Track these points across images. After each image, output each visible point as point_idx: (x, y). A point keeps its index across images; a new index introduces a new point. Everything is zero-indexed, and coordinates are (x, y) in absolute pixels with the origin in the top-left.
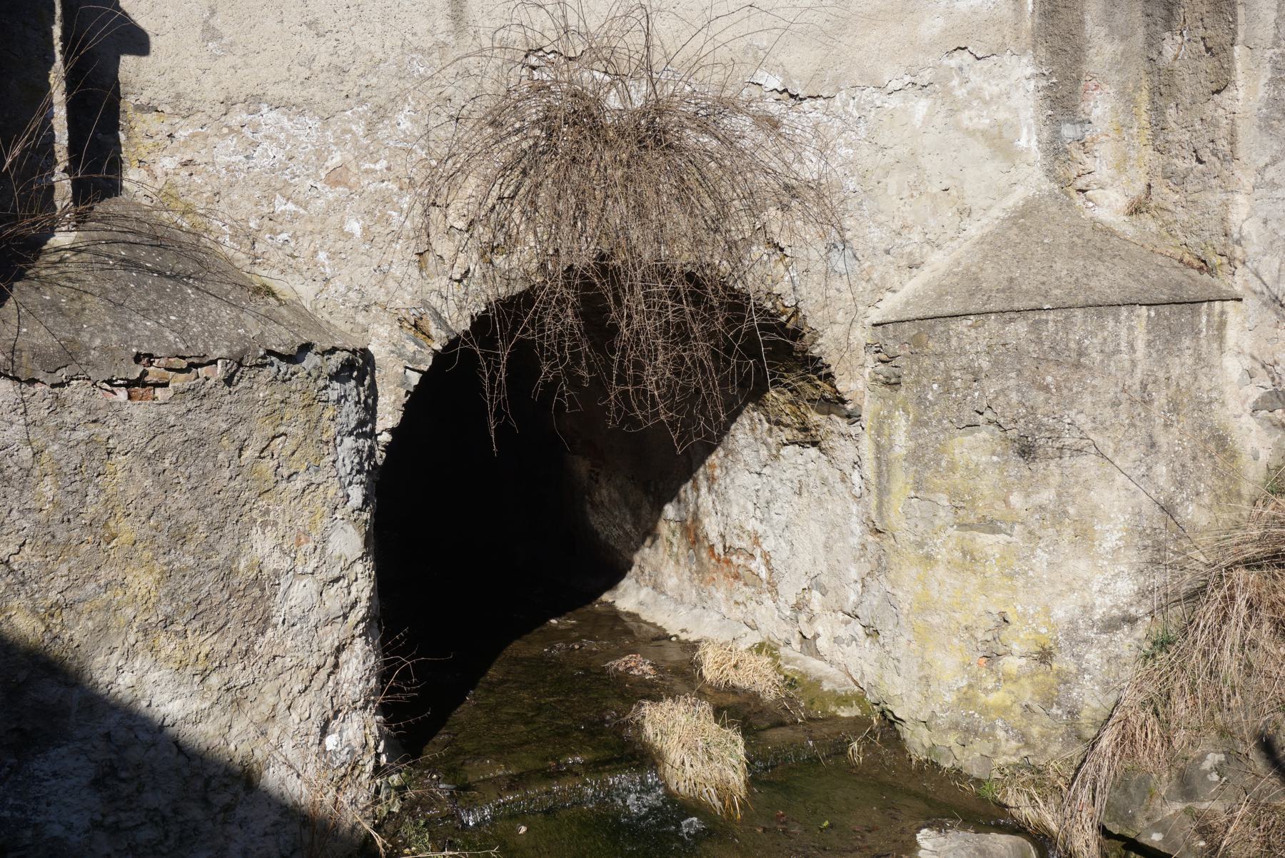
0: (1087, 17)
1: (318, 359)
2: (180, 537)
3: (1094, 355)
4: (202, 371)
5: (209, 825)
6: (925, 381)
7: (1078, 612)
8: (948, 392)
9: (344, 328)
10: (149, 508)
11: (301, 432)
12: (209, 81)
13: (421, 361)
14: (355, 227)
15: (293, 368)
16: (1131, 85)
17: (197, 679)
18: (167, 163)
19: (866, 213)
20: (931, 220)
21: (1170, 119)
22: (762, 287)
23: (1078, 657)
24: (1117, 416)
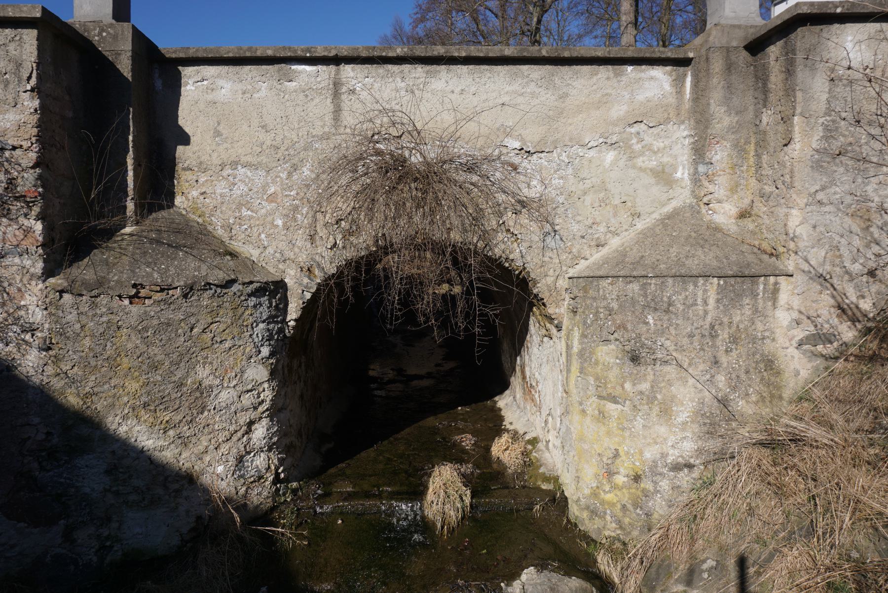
0: (712, 101)
1: (241, 287)
2: (155, 367)
3: (679, 305)
4: (171, 292)
5: (167, 497)
6: (587, 312)
7: (658, 456)
8: (596, 320)
9: (273, 272)
10: (138, 353)
11: (229, 321)
12: (215, 155)
13: (311, 288)
14: (279, 222)
15: (225, 291)
16: (742, 141)
17: (161, 431)
18: (195, 193)
19: (570, 216)
20: (613, 220)
21: (764, 162)
22: (503, 255)
23: (655, 483)
24: (691, 343)
